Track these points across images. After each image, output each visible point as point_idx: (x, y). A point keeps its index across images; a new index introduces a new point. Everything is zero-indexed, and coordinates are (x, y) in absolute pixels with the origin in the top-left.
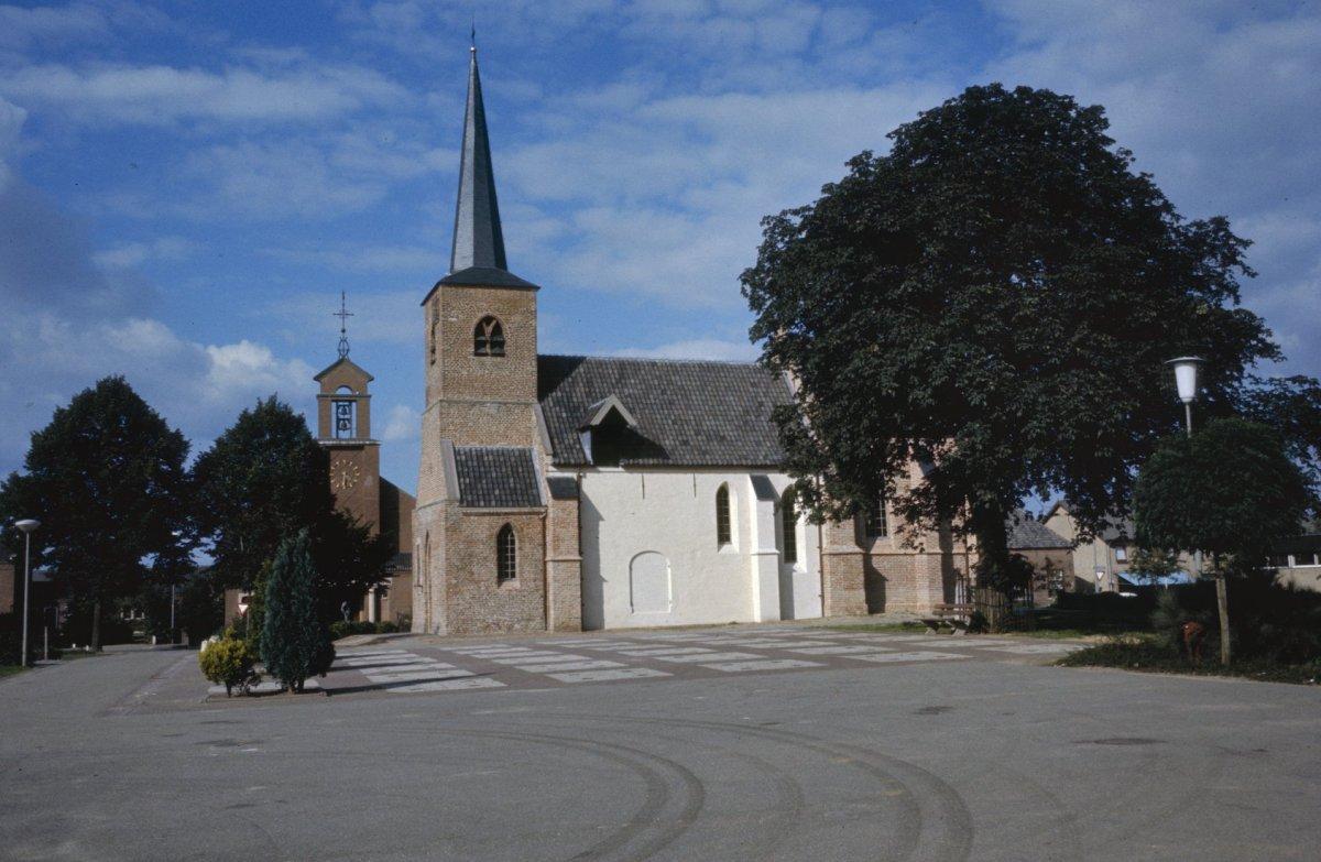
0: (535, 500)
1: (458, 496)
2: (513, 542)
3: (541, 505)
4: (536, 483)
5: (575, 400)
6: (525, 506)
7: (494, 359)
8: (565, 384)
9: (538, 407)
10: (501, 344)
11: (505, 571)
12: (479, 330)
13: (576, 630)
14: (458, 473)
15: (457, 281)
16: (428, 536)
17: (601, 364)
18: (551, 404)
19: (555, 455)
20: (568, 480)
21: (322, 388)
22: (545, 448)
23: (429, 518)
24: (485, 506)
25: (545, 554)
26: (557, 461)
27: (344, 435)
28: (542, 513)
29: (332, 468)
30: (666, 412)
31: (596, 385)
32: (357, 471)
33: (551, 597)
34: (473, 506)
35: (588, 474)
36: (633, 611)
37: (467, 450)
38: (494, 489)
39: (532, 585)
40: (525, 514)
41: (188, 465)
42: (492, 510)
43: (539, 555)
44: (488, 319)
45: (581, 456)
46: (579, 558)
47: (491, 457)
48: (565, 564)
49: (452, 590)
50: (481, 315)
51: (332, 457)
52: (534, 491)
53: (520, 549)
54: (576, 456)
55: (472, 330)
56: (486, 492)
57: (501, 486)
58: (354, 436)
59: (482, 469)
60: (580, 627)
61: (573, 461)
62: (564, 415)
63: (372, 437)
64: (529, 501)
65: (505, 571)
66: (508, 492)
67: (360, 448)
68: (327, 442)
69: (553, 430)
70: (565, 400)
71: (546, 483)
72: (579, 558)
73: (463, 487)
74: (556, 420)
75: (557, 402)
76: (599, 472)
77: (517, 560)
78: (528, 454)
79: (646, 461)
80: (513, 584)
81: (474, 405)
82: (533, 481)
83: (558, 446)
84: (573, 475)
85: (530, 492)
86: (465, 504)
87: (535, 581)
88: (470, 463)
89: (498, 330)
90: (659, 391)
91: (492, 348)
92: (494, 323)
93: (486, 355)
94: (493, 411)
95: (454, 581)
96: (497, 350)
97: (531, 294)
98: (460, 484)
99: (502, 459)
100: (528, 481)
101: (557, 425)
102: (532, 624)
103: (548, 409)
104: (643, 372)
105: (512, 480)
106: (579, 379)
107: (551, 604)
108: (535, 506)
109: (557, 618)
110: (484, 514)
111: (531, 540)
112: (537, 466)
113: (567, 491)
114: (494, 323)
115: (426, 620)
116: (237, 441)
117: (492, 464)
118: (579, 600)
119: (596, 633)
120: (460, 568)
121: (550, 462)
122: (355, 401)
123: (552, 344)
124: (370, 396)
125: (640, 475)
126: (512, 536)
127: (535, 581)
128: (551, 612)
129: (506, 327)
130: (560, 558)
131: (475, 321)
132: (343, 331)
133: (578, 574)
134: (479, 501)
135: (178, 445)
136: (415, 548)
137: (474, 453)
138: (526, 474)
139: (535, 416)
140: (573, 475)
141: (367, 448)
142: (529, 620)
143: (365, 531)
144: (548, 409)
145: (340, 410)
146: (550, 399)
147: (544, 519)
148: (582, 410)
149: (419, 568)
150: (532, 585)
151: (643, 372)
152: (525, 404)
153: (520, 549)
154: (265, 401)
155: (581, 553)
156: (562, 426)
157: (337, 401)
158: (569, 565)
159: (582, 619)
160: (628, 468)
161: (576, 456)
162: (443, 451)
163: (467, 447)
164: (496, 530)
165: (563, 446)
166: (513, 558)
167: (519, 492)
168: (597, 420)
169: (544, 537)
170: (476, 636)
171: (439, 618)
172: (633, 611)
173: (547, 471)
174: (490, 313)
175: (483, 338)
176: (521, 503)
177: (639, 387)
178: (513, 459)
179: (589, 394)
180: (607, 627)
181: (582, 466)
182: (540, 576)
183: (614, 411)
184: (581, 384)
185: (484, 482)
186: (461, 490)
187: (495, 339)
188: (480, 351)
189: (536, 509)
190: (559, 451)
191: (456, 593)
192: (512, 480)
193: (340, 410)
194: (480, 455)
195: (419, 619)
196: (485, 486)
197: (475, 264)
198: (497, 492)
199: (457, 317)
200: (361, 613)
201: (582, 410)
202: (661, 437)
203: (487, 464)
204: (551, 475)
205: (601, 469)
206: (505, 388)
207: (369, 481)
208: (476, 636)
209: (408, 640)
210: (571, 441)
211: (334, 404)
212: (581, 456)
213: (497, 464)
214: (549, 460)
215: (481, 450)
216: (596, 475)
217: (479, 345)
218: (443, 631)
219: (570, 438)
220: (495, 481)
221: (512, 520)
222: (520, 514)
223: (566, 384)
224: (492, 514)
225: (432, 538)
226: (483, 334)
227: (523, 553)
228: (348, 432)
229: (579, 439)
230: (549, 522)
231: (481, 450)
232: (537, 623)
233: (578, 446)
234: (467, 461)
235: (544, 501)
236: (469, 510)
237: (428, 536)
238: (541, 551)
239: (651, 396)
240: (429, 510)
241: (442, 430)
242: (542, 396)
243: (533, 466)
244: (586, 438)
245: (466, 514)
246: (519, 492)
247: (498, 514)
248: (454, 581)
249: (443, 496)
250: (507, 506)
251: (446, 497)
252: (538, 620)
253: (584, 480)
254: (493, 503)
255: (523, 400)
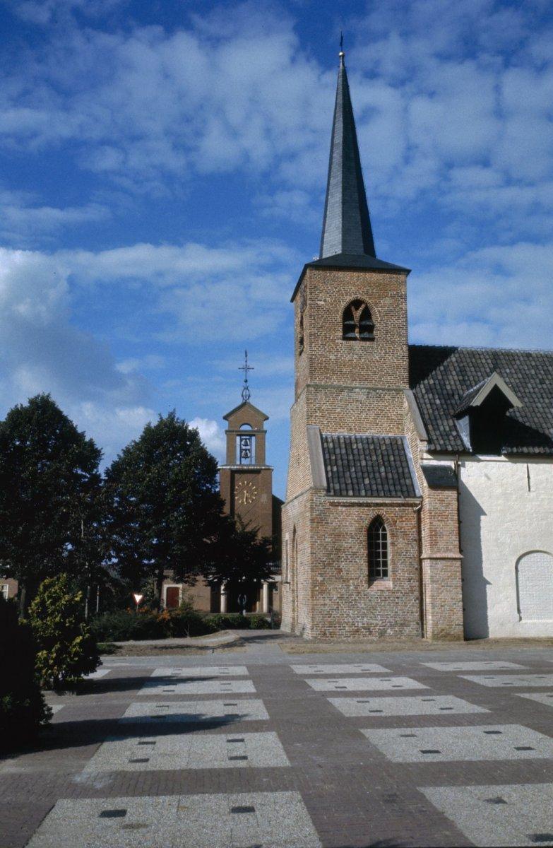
0: (409, 491)
1: (325, 484)
2: (385, 537)
3: (415, 496)
4: (409, 472)
5: (448, 387)
6: (397, 497)
7: (363, 343)
8: (438, 372)
9: (410, 393)
10: (370, 329)
11: (376, 569)
12: (347, 314)
13: (458, 639)
14: (325, 461)
15: (324, 265)
16: (295, 531)
17: (473, 354)
18: (424, 391)
19: (430, 441)
20: (445, 469)
21: (230, 426)
22: (420, 435)
23: (296, 512)
24: (354, 496)
25: (420, 552)
26: (433, 447)
27: (244, 461)
28: (416, 505)
29: (236, 487)
30: (547, 401)
31: (469, 373)
32: (255, 490)
33: (428, 600)
34: (341, 495)
35: (467, 463)
36: (521, 619)
37: (335, 437)
38: (363, 478)
39: (406, 585)
40: (399, 505)
41: (102, 468)
42: (361, 500)
43: (414, 552)
44: (357, 303)
45: (459, 442)
46: (459, 556)
47: (360, 446)
48: (444, 562)
49: (318, 589)
50: (349, 299)
51: (236, 479)
52: (408, 481)
53: (393, 544)
54: (452, 443)
55: (341, 313)
56: (355, 481)
57: (371, 476)
58: (253, 462)
59: (351, 457)
60: (462, 636)
61: (450, 448)
62: (438, 402)
63: (267, 463)
64: (402, 491)
65: (376, 569)
66: (379, 481)
67: (258, 472)
68: (232, 467)
69: (427, 417)
70: (438, 387)
71: (421, 472)
72: (459, 556)
73: (330, 474)
74: (429, 406)
75: (430, 389)
76: (479, 461)
77: (389, 557)
78: (400, 443)
79: (531, 450)
80: (385, 584)
81: (342, 390)
82: (406, 470)
83: (432, 433)
84: (450, 463)
85: (402, 481)
86: (332, 493)
87: (409, 580)
88: (338, 451)
89: (367, 314)
90: (538, 381)
91: (360, 332)
92: (363, 306)
93: (355, 339)
94: (362, 397)
95: (320, 579)
96: (366, 335)
97: (401, 277)
98: (327, 472)
99: (372, 447)
100: (400, 470)
101: (431, 411)
102: (407, 630)
103: (420, 395)
104: (518, 362)
105: (382, 469)
106: (452, 368)
107: (428, 608)
108: (409, 496)
109: (435, 625)
110: (353, 505)
111: (405, 534)
112: (410, 455)
113: (444, 480)
114: (363, 306)
115: (293, 619)
116: (139, 449)
117: (362, 452)
118: (461, 604)
119: (482, 641)
120: (327, 563)
121: (425, 449)
122: (254, 435)
123: (424, 334)
124: (266, 432)
125: (525, 465)
126: (384, 529)
127: (409, 580)
128: (429, 618)
129: (375, 311)
130: (438, 555)
131: (343, 305)
132: (246, 381)
133: (459, 574)
134: (347, 491)
135: (91, 454)
136: (284, 544)
137: (342, 441)
138: (398, 463)
139: (407, 401)
140: (450, 463)
141: (262, 472)
142: (402, 625)
143: (253, 535)
144: (420, 395)
145: (243, 443)
146: (422, 386)
147: (419, 512)
148: (456, 397)
149: (287, 564)
150: (406, 585)
151: (518, 362)
152: (396, 390)
153: (393, 544)
154: (165, 416)
155: (461, 551)
156: (436, 413)
157: (240, 435)
158: (449, 563)
159: (465, 625)
160: (513, 457)
161: (452, 443)
162: (310, 442)
163: (335, 435)
164: (366, 523)
165: (438, 433)
166: (385, 555)
167: (391, 482)
168: (477, 401)
169: (419, 532)
170: (343, 642)
171: (305, 619)
172: (521, 619)
173: (422, 459)
174: (359, 296)
175: (352, 322)
176: (394, 493)
177: (515, 376)
178: (384, 448)
179: (463, 382)
180: (491, 636)
181: (461, 454)
182: (415, 576)
183: (496, 391)
184: (454, 373)
185: (353, 470)
186: (327, 478)
187: (363, 323)
188: (347, 336)
189: (410, 500)
190: (435, 438)
191: (322, 592)
192: (382, 469)
193: (243, 443)
194: (348, 443)
195: (287, 618)
196: (354, 475)
197: (343, 250)
198: (367, 481)
199: (325, 301)
200: (258, 603)
201: (456, 397)
202: (544, 425)
203: (356, 452)
204: (426, 462)
205: (482, 458)
206: (375, 373)
207: (265, 499)
208: (343, 642)
209: (271, 645)
210: (447, 429)
211: (238, 439)
212: (459, 442)
213: (367, 452)
214: (424, 446)
215: (350, 438)
216: (475, 464)
217: (347, 329)
218: (308, 635)
219: (445, 425)
220: (365, 470)
221: (383, 511)
222: (392, 505)
223: (439, 373)
224: (360, 505)
225: (299, 533)
226: (352, 319)
227: (396, 549)
228: (248, 460)
229: (455, 426)
230: (425, 516)
231: (350, 438)
232: (412, 629)
233: (454, 433)
234: (334, 448)
235: (419, 492)
236: (337, 500)
237: (295, 531)
238: (416, 548)
239: (529, 385)
240: (296, 502)
241: (309, 417)
242: (413, 383)
243: (405, 455)
244: (464, 425)
245: (332, 504)
246: (391, 482)
247: (368, 505)
248: (320, 579)
249: (309, 484)
250: (378, 496)
251: (312, 485)
252: (414, 626)
253: (462, 470)
254: (363, 493)
255: (392, 386)
